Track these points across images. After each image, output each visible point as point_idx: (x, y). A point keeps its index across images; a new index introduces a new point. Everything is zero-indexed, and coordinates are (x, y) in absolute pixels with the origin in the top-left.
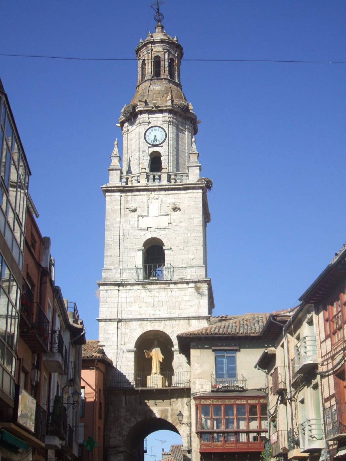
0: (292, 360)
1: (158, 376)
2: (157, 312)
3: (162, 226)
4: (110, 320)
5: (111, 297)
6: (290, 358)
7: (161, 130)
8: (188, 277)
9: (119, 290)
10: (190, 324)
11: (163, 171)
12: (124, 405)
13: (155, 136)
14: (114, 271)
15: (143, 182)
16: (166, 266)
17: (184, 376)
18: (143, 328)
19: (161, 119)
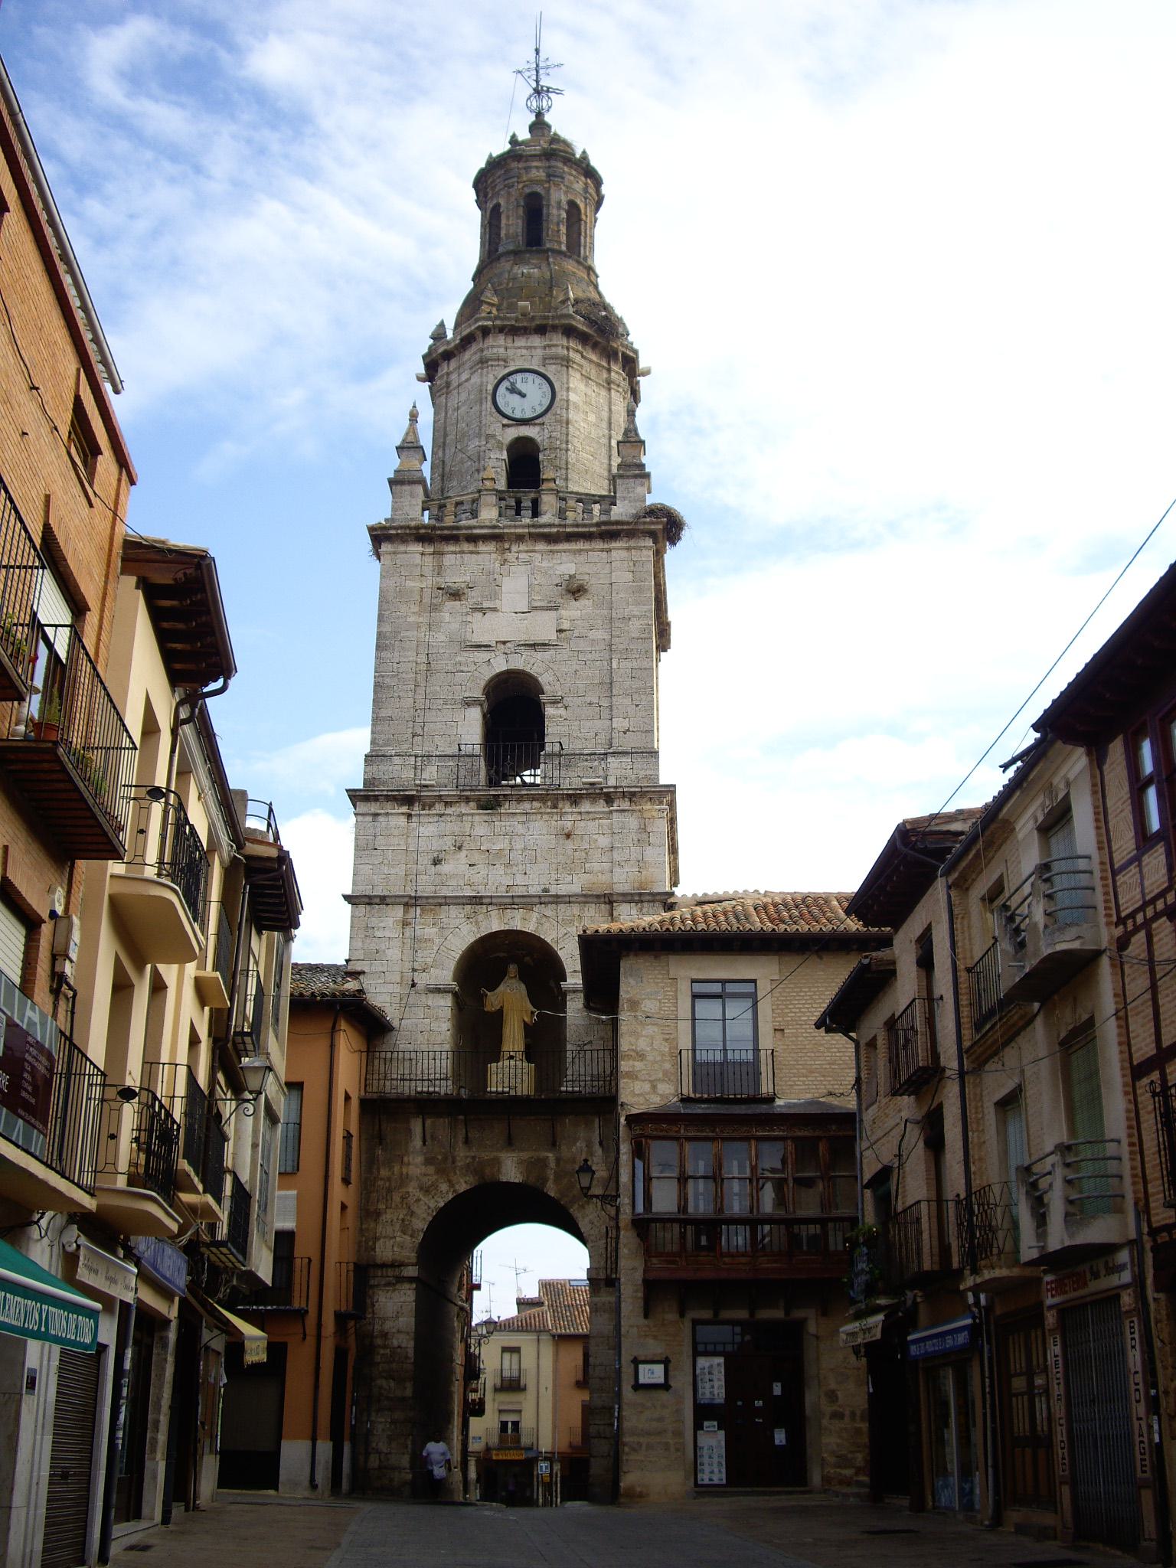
0: (969, 970)
1: (519, 1063)
2: (520, 880)
3: (539, 639)
4: (383, 900)
6: (961, 966)
7: (539, 380)
8: (612, 782)
9: (409, 816)
10: (615, 914)
11: (544, 486)
12: (417, 1142)
13: (523, 396)
14: (397, 760)
15: (489, 514)
16: (548, 748)
17: (595, 1064)
19: (539, 352)
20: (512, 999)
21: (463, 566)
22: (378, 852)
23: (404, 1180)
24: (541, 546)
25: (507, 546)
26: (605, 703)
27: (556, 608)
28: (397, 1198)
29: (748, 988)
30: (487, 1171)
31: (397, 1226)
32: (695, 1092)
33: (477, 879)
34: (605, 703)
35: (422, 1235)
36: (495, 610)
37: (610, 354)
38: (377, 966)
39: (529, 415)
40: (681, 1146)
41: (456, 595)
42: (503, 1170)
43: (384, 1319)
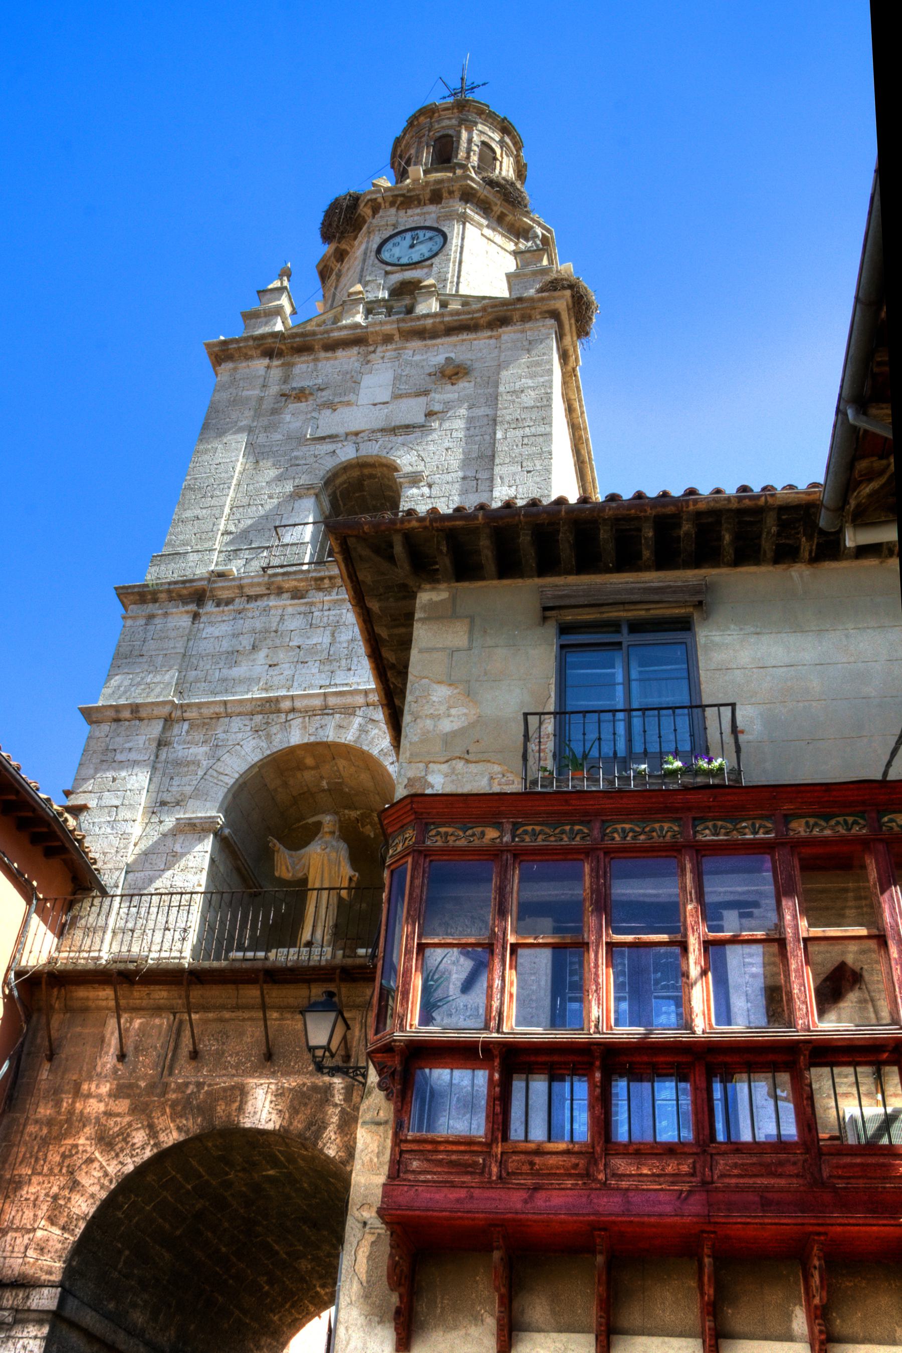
5: (161, 639)
12: (108, 1060)
18: (269, 736)
22: (144, 659)
23: (71, 1123)
24: (416, 344)
25: (371, 348)
27: (426, 393)
30: (220, 1108)
35: (82, 1225)
42: (249, 1108)
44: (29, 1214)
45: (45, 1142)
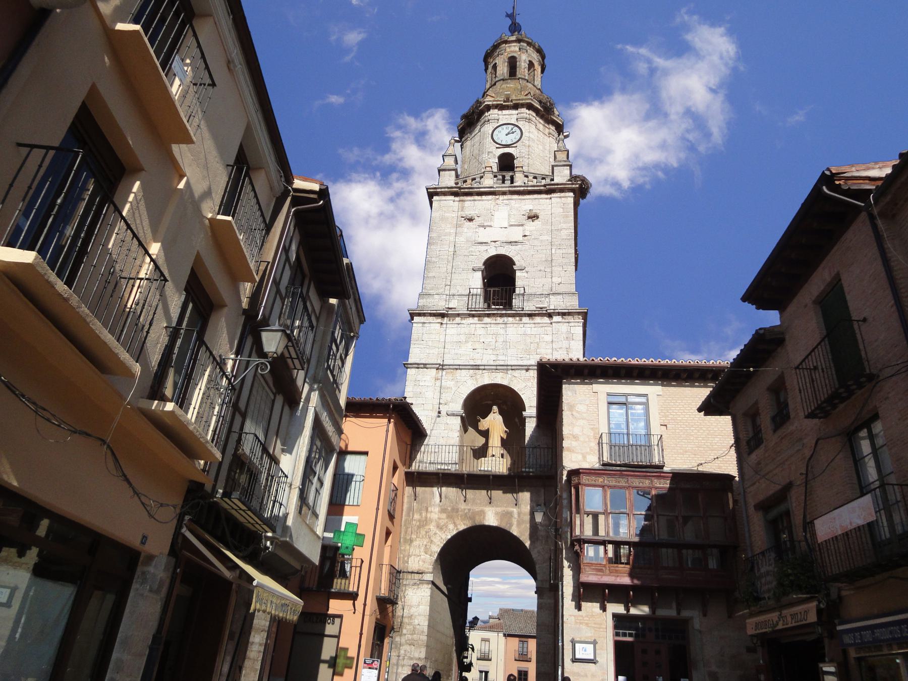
8: (552, 307)
16: (517, 291)
19: (516, 117)
20: (494, 422)
21: (474, 206)
23: (424, 523)
26: (548, 270)
27: (522, 225)
28: (423, 532)
29: (643, 400)
30: (477, 518)
31: (422, 549)
32: (611, 459)
33: (477, 356)
34: (548, 270)
36: (491, 226)
37: (549, 121)
38: (420, 401)
39: (509, 143)
40: (605, 492)
41: (471, 220)
43: (411, 606)
44: (418, 550)
45: (419, 527)
